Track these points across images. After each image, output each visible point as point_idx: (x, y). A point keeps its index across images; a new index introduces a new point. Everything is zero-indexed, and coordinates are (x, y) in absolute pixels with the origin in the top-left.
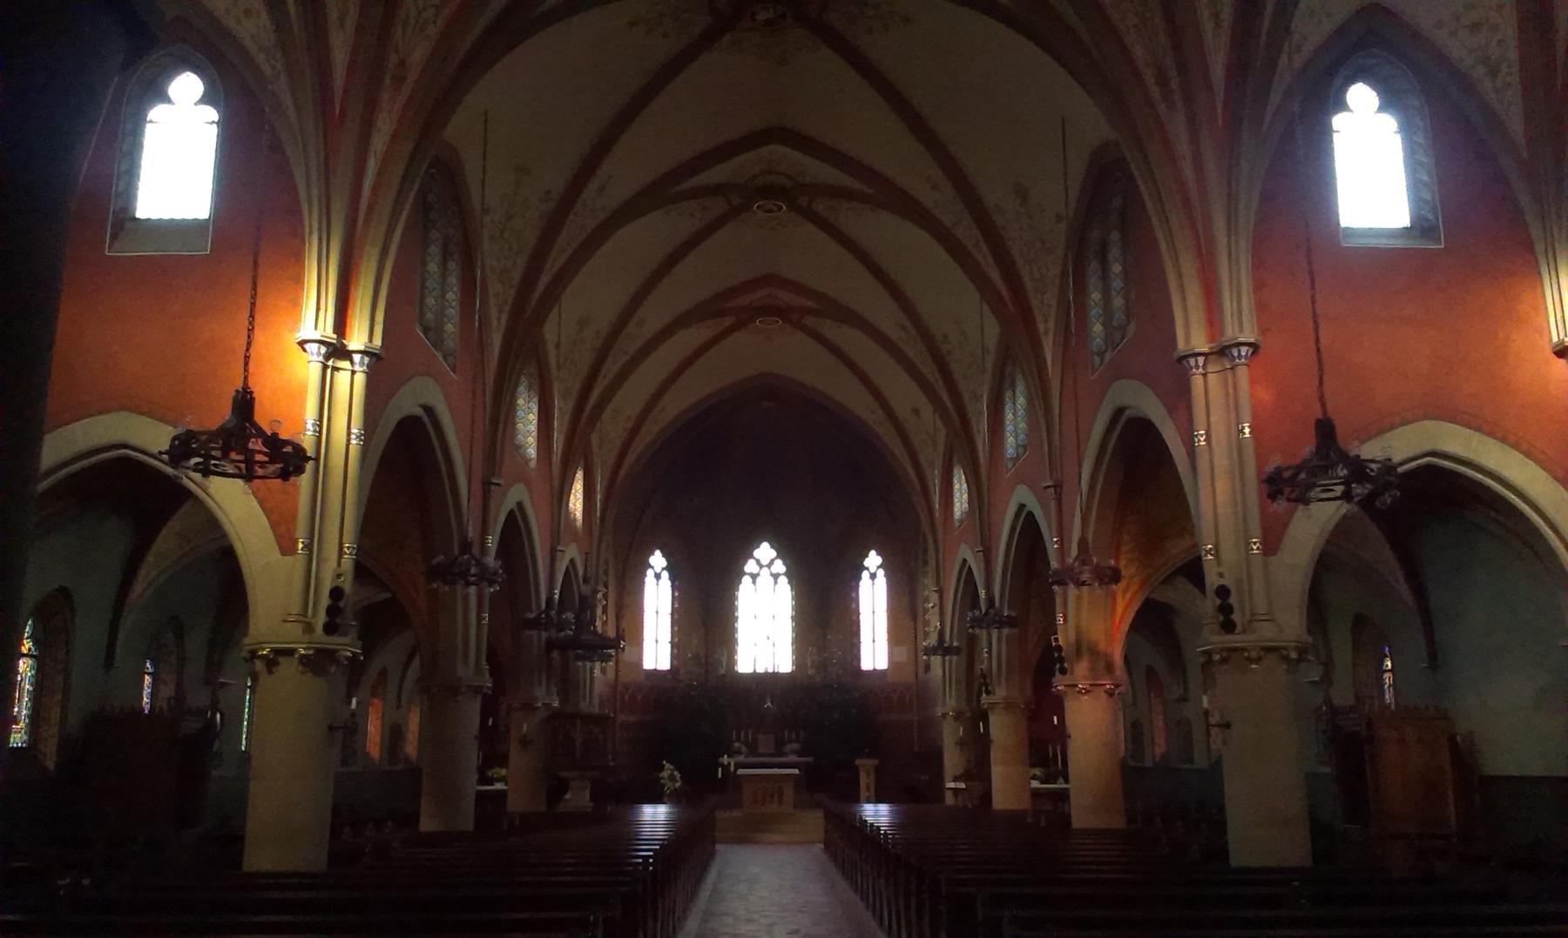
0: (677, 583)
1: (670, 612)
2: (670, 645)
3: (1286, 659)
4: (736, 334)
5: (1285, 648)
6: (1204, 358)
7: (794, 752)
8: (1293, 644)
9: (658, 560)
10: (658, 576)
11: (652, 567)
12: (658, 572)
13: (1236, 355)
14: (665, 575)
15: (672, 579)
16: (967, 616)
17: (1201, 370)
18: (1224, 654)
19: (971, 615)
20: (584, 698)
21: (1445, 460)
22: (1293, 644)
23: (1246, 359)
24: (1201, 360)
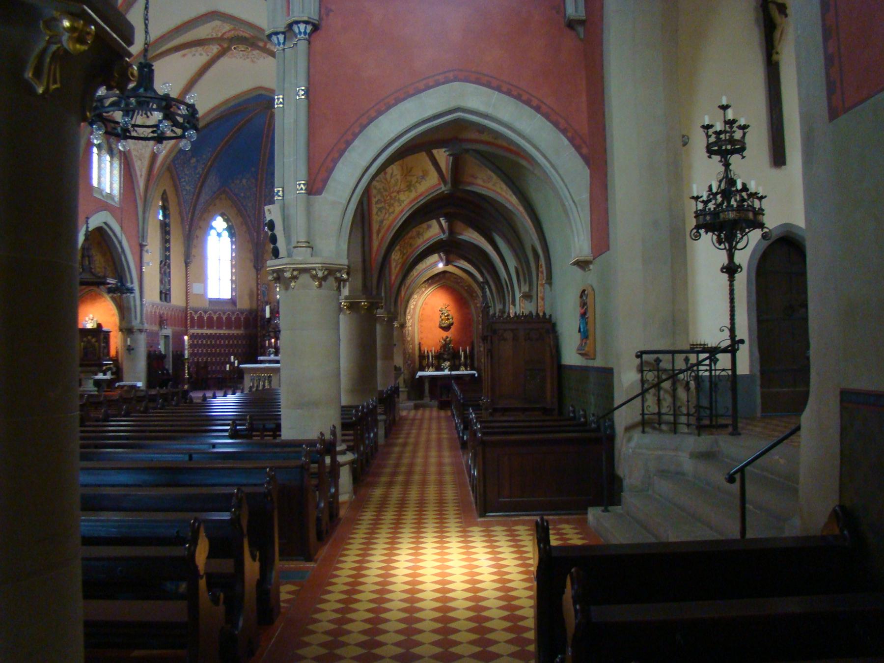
0: (234, 240)
1: (230, 259)
2: (230, 281)
3: (314, 277)
4: (222, 59)
5: (314, 269)
6: (283, 36)
7: (499, 314)
8: (320, 265)
9: (219, 223)
10: (219, 235)
11: (215, 229)
12: (219, 232)
13: (297, 31)
14: (226, 234)
15: (232, 235)
16: (725, 234)
17: (282, 46)
18: (295, 273)
19: (722, 235)
20: (136, 318)
21: (486, 119)
22: (320, 265)
23: (305, 35)
24: (281, 37)
